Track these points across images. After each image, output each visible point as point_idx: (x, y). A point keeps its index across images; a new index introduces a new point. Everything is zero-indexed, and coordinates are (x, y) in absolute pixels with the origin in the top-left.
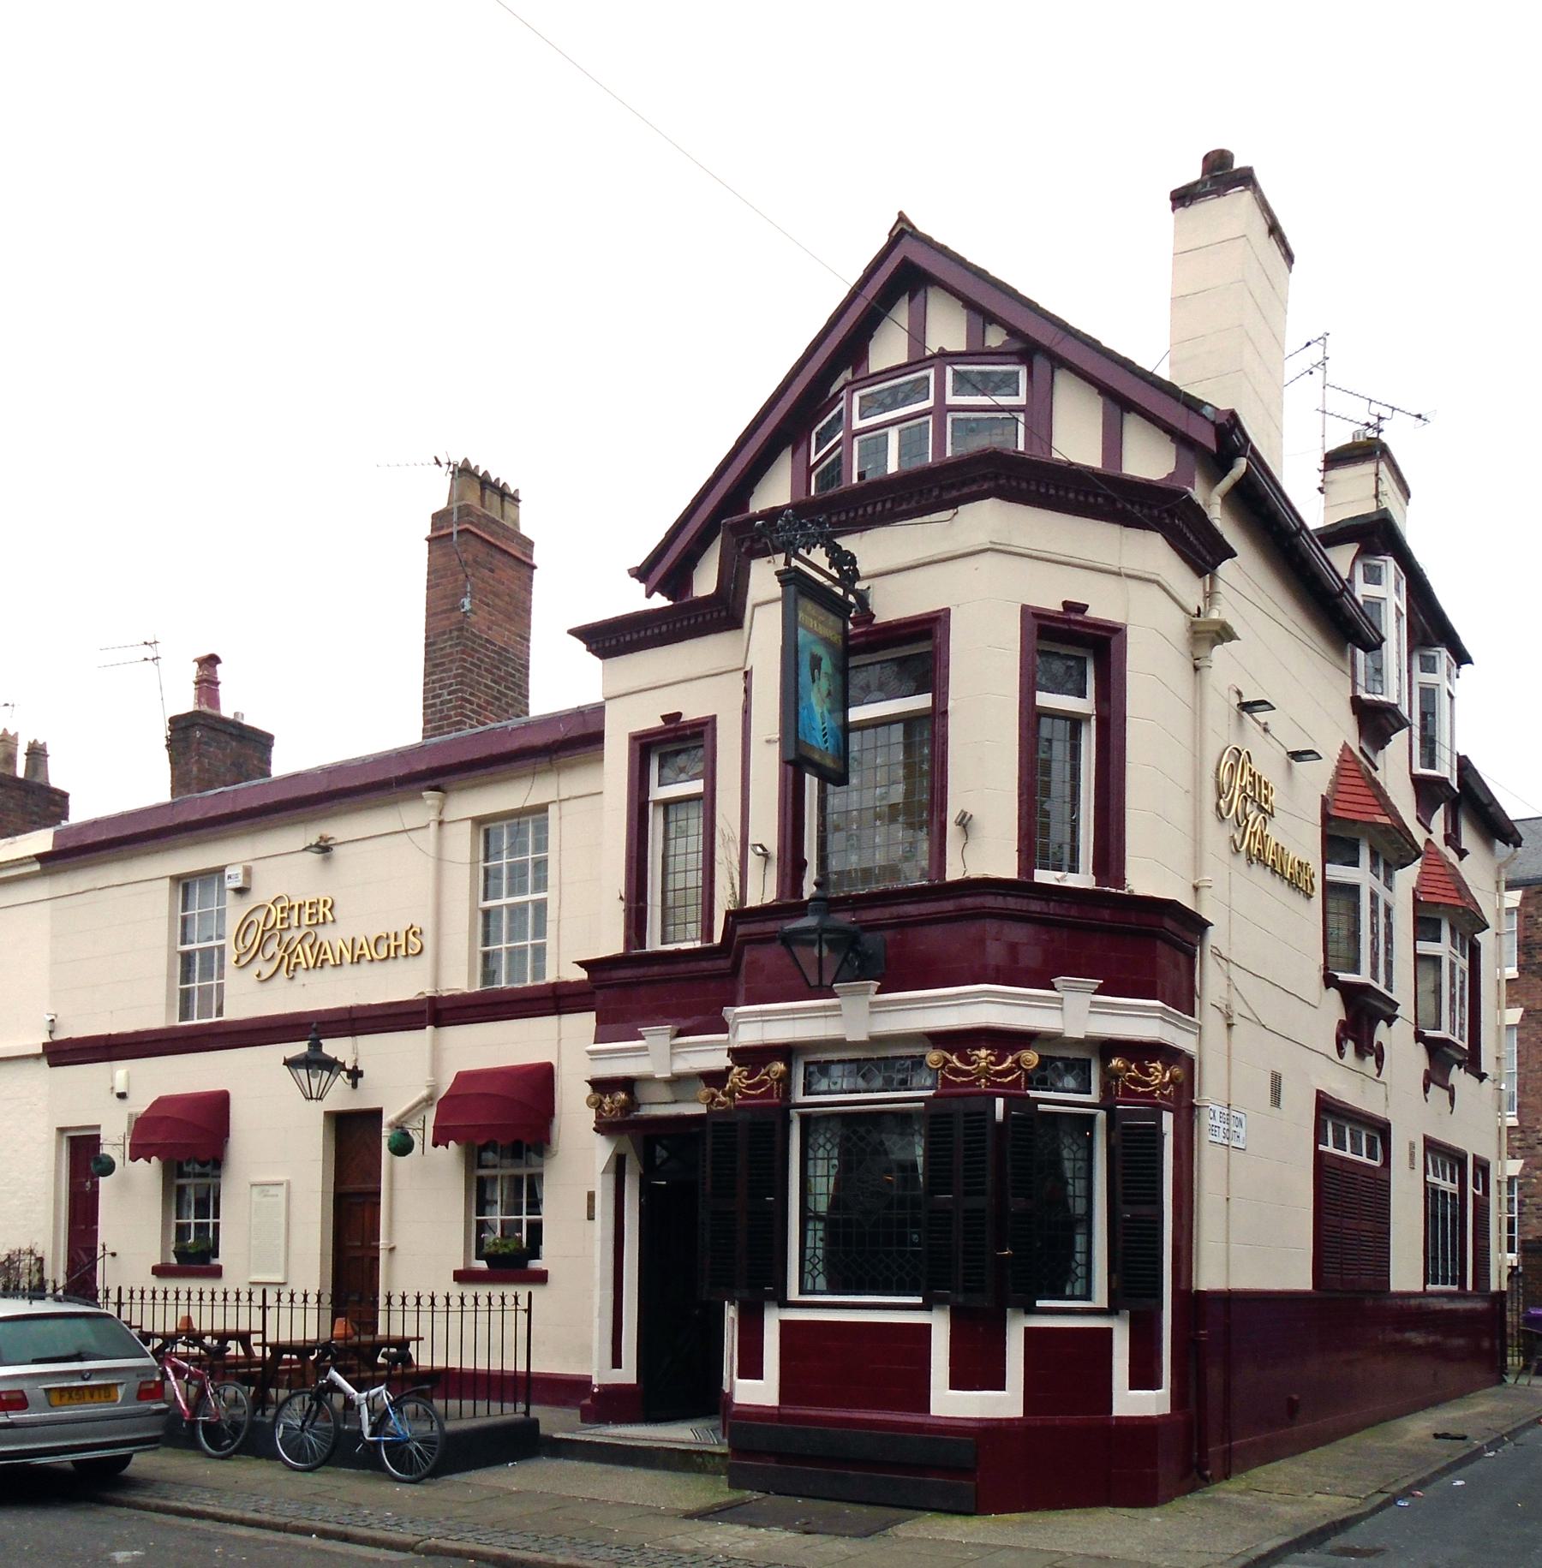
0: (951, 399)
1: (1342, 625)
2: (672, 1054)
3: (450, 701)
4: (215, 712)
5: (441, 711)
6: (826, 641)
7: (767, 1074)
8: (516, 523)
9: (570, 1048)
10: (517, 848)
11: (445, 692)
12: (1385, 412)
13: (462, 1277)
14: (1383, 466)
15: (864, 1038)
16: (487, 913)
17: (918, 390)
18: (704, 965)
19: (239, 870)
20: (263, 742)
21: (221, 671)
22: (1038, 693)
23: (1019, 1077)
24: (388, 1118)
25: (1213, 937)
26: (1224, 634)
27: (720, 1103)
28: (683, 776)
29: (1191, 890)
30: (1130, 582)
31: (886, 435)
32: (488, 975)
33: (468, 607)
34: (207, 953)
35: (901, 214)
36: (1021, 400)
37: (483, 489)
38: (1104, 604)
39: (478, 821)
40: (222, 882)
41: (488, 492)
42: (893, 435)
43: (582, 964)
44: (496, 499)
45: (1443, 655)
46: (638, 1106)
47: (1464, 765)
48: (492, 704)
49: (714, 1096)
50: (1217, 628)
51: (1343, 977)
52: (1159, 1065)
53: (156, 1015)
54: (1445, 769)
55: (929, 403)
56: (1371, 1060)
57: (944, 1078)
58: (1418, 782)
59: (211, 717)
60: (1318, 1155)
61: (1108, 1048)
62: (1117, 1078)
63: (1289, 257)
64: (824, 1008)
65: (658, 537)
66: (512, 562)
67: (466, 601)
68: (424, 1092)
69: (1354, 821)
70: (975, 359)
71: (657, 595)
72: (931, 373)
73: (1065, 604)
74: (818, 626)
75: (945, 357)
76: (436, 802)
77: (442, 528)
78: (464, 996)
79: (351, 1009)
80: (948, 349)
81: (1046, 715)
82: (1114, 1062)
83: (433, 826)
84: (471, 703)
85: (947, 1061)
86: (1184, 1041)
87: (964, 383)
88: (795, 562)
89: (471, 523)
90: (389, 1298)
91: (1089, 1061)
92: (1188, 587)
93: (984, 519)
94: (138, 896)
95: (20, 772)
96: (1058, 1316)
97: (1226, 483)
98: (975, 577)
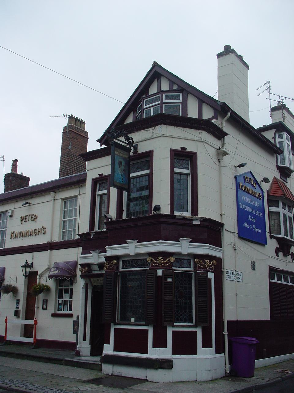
0: (164, 101)
2: (98, 258)
3: (65, 170)
4: (16, 173)
5: (63, 172)
6: (124, 159)
7: (112, 263)
8: (84, 129)
9: (73, 255)
11: (64, 168)
15: (133, 254)
16: (64, 222)
17: (157, 99)
20: (27, 180)
23: (170, 264)
24: (39, 273)
25: (226, 227)
26: (225, 153)
28: (104, 189)
29: (220, 216)
31: (151, 109)
35: (154, 61)
36: (181, 101)
37: (76, 121)
38: (191, 148)
39: (63, 199)
41: (77, 122)
42: (152, 109)
46: (92, 271)
48: (76, 170)
50: (223, 152)
51: (275, 235)
52: (208, 261)
55: (159, 102)
59: (15, 174)
60: (270, 283)
61: (196, 256)
62: (197, 264)
63: (247, 67)
67: (70, 147)
68: (47, 267)
69: (277, 196)
70: (171, 92)
73: (181, 148)
76: (53, 195)
77: (66, 130)
78: (57, 242)
81: (175, 174)
82: (196, 260)
83: (53, 200)
84: (70, 170)
86: (218, 254)
89: (72, 129)
92: (217, 143)
93: (163, 129)
96: (183, 327)
97: (226, 118)
98: (160, 143)
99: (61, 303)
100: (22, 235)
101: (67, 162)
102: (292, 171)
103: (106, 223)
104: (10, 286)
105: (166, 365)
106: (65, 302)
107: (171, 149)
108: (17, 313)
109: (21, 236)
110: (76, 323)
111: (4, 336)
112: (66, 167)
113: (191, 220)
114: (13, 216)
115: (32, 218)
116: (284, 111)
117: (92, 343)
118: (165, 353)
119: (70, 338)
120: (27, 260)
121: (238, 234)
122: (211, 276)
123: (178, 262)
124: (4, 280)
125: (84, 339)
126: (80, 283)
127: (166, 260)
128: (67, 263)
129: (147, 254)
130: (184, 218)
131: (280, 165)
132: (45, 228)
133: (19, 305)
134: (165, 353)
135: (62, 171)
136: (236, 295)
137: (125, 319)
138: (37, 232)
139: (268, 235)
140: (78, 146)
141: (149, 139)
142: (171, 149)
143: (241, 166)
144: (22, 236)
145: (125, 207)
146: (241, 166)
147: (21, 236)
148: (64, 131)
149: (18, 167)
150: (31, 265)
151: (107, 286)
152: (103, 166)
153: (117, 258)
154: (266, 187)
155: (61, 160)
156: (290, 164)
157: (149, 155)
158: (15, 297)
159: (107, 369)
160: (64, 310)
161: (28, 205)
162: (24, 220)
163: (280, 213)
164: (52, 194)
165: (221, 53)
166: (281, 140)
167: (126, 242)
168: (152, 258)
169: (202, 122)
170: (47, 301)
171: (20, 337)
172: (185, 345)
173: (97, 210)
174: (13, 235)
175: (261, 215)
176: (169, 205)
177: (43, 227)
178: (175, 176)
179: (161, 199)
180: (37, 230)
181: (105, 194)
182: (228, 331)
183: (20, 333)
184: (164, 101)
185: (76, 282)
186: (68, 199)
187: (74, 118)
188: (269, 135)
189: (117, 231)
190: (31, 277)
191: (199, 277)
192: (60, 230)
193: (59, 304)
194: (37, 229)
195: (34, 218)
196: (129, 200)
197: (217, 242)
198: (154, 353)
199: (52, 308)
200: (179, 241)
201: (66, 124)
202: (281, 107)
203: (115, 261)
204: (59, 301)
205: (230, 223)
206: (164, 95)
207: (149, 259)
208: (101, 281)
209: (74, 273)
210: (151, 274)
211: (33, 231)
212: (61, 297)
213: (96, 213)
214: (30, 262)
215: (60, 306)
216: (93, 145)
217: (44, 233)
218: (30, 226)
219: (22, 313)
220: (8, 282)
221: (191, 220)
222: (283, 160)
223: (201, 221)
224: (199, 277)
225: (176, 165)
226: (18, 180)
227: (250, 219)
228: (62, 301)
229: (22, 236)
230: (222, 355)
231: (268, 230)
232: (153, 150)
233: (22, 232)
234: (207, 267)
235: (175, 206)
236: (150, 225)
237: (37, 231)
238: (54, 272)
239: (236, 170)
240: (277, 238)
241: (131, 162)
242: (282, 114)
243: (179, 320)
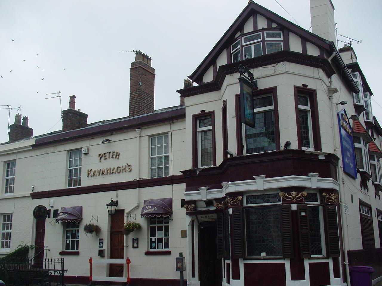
0: (266, 39)
1: (351, 88)
2: (207, 194)
3: (136, 107)
5: (134, 109)
7: (237, 199)
9: (178, 193)
11: (135, 104)
12: (352, 41)
13: (62, 253)
14: (352, 52)
15: (262, 189)
16: (152, 159)
17: (258, 37)
18: (214, 171)
19: (86, 149)
20: (85, 116)
21: (76, 100)
22: (299, 105)
23: (302, 198)
24: (126, 211)
26: (335, 91)
27: (220, 207)
28: (206, 125)
29: (334, 150)
30: (316, 80)
31: (251, 46)
33: (141, 84)
34: (76, 170)
36: (282, 39)
37: (143, 57)
39: (150, 136)
40: (81, 151)
41: (144, 58)
42: (253, 47)
43: (182, 172)
44: (146, 59)
47: (374, 118)
48: (146, 107)
49: (218, 205)
52: (334, 194)
53: (62, 185)
54: (371, 120)
55: (261, 40)
57: (326, 200)
58: (366, 122)
59: (73, 110)
63: (334, 8)
64: (252, 182)
65: (195, 69)
67: (140, 83)
72: (261, 33)
74: (247, 89)
75: (263, 30)
76: (139, 132)
78: (147, 180)
79: (116, 184)
80: (264, 28)
83: (138, 137)
85: (285, 195)
86: (337, 188)
87: (268, 35)
88: (242, 76)
89: (141, 65)
90: (46, 260)
91: (317, 194)
94: (58, 157)
98: (283, 80)
99: (69, 242)
100: (102, 173)
101: (138, 99)
104: (93, 225)
106: (160, 240)
107: (294, 86)
108: (101, 253)
109: (101, 174)
111: (89, 277)
112: (137, 103)
114: (88, 153)
115: (113, 155)
120: (112, 199)
124: (82, 219)
125: (193, 276)
127: (298, 195)
129: (279, 189)
132: (131, 166)
133: (103, 244)
135: (132, 108)
136: (347, 227)
138: (120, 170)
140: (147, 83)
141: (271, 76)
142: (294, 86)
144: (102, 174)
145: (244, 144)
147: (101, 174)
148: (131, 67)
149: (75, 103)
151: (235, 222)
152: (204, 103)
155: (130, 97)
157: (273, 91)
158: (99, 236)
160: (158, 248)
161: (108, 142)
162: (103, 158)
163: (362, 149)
164: (138, 131)
167: (254, 177)
168: (284, 193)
169: (320, 60)
170: (137, 239)
171: (106, 277)
173: (199, 146)
174: (90, 173)
176: (297, 141)
177: (127, 164)
179: (288, 134)
180: (120, 167)
182: (348, 261)
183: (106, 273)
185: (172, 219)
186: (163, 134)
187: (142, 54)
189: (238, 167)
191: (328, 210)
193: (152, 242)
194: (121, 167)
195: (117, 155)
199: (144, 245)
200: (308, 176)
201: (133, 60)
203: (240, 197)
204: (66, 241)
207: (282, 194)
208: (209, 218)
209: (170, 210)
210: (286, 208)
211: (116, 169)
212: (153, 234)
213: (199, 150)
214: (115, 200)
215: (153, 244)
217: (130, 171)
219: (107, 253)
220: (91, 221)
221: (317, 156)
222: (359, 101)
223: (325, 156)
224: (328, 210)
226: (77, 117)
228: (155, 239)
229: (102, 174)
232: (276, 87)
233: (102, 170)
234: (333, 201)
237: (121, 169)
238: (149, 210)
242: (351, 55)
243: (277, 253)
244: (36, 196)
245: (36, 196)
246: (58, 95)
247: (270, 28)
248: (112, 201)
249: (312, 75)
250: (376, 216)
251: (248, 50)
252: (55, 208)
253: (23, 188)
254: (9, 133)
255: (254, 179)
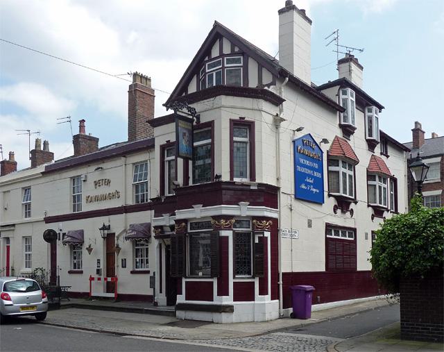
0: (226, 65)
8: (150, 86)
9: (147, 217)
10: (141, 170)
12: (351, 50)
17: (219, 63)
19: (83, 176)
20: (96, 140)
24: (116, 235)
25: (282, 190)
26: (283, 120)
32: (137, 201)
36: (242, 64)
38: (249, 117)
39: (134, 164)
45: (374, 108)
54: (376, 137)
55: (221, 66)
56: (348, 213)
60: (327, 240)
61: (254, 218)
66: (148, 96)
71: (170, 109)
79: (108, 209)
86: (275, 215)
87: (229, 61)
92: (273, 110)
93: (225, 100)
94: (63, 183)
95: (42, 149)
97: (284, 83)
98: (223, 112)
100: (97, 199)
102: (355, 129)
103: (174, 190)
105: (229, 309)
110: (153, 278)
113: (249, 186)
116: (352, 64)
117: (168, 294)
118: (227, 300)
119: (149, 292)
121: (295, 195)
122: (267, 234)
123: (238, 223)
125: (161, 292)
126: (154, 244)
128: (142, 225)
130: (242, 184)
131: (343, 123)
134: (227, 300)
137: (193, 274)
138: (116, 195)
139: (326, 194)
143: (299, 130)
146: (299, 130)
150: (109, 228)
153: (186, 221)
154: (325, 148)
156: (353, 122)
159: (181, 314)
165: (283, 9)
166: (345, 97)
172: (244, 293)
175: (319, 175)
178: (235, 144)
179: (223, 169)
181: (173, 160)
184: (226, 65)
188: (330, 94)
189: (185, 197)
190: (109, 238)
192: (133, 194)
195: (108, 182)
196: (194, 167)
197: (274, 204)
198: (219, 300)
202: (349, 59)
205: (287, 186)
206: (225, 58)
214: (107, 224)
216: (160, 111)
217: (119, 197)
218: (103, 190)
222: (345, 118)
225: (236, 134)
227: (308, 181)
230: (277, 301)
231: (326, 188)
235: (235, 173)
236: (213, 192)
239: (294, 134)
240: (335, 197)
241: (182, 160)
244: (48, 220)
245: (48, 220)
246: (68, 119)
247: (233, 53)
248: (104, 225)
249: (251, 107)
250: (366, 238)
251: (211, 77)
252: (64, 232)
253: (37, 215)
254: (30, 159)
255: (193, 208)
